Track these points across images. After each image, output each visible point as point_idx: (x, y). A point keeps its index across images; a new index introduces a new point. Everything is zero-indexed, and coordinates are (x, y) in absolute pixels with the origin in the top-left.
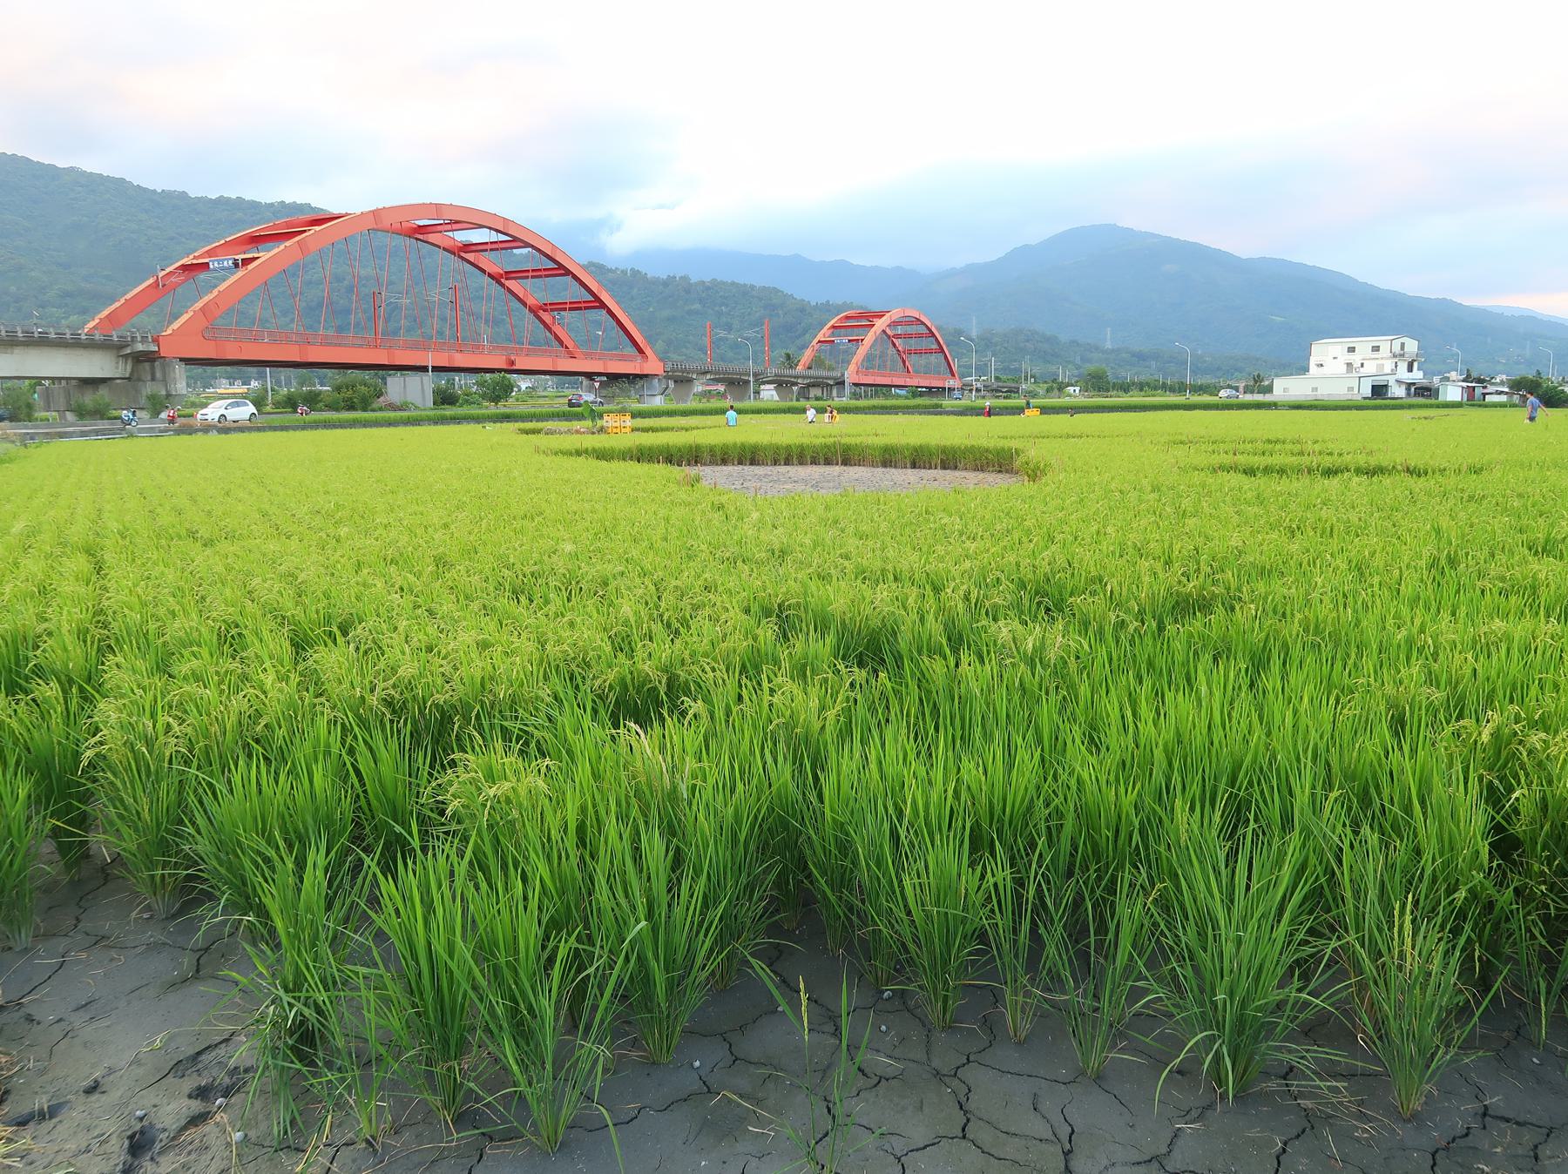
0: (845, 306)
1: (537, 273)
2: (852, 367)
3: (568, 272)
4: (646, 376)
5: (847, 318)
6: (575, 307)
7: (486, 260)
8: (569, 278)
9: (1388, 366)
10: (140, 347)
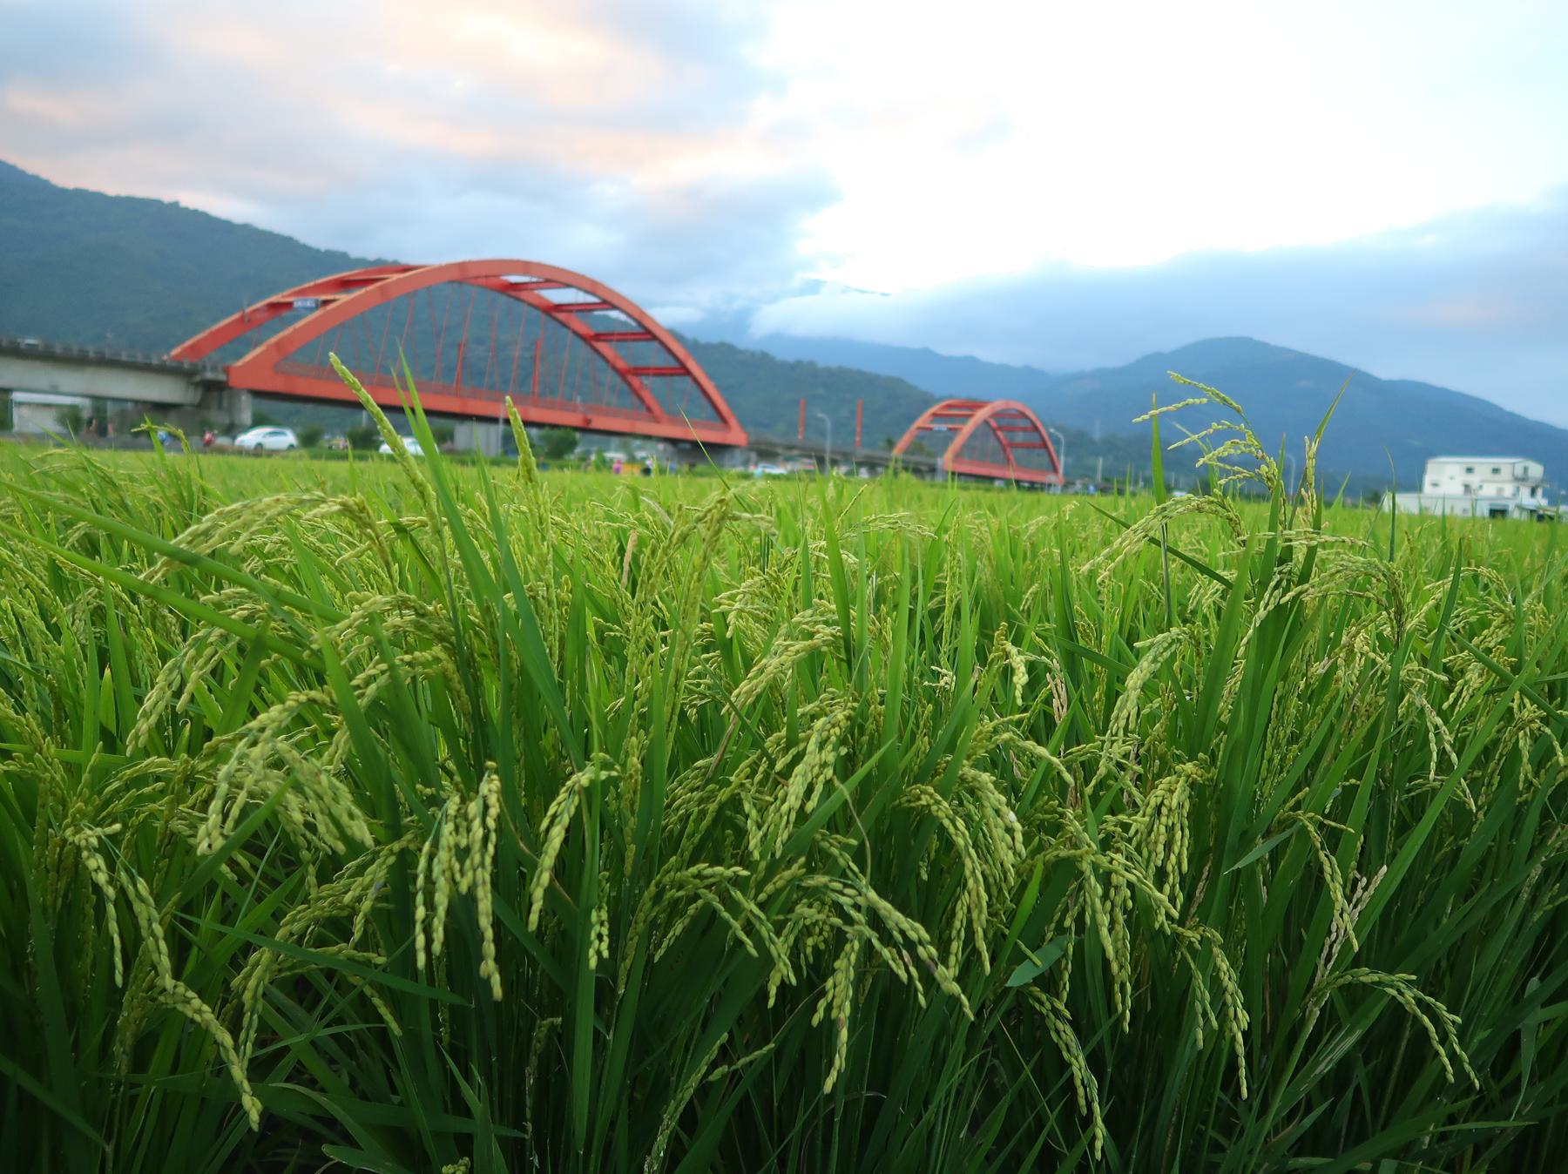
0: (951, 397)
1: (624, 337)
2: (949, 455)
5: (949, 407)
6: (660, 372)
7: (577, 322)
8: (655, 344)
9: (1509, 490)
10: (209, 375)
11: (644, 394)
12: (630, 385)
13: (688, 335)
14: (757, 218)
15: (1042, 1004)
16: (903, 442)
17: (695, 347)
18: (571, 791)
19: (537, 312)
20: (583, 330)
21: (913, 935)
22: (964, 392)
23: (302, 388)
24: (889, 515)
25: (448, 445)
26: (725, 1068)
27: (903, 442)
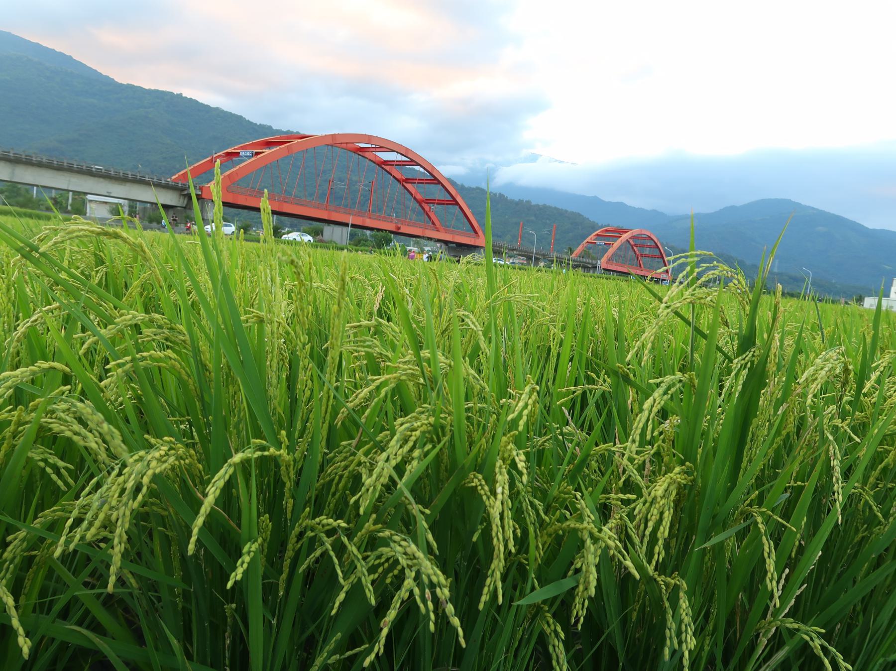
0: (608, 225)
1: (422, 181)
2: (604, 259)
3: (439, 183)
4: (478, 247)
5: (607, 231)
6: (441, 203)
7: (395, 171)
11: (431, 214)
12: (423, 209)
13: (459, 182)
14: (502, 117)
15: (549, 625)
16: (578, 250)
17: (462, 189)
18: (230, 466)
19: (373, 165)
20: (398, 176)
21: (434, 579)
22: (615, 223)
24: (549, 295)
25: (319, 237)
26: (338, 656)
27: (578, 250)
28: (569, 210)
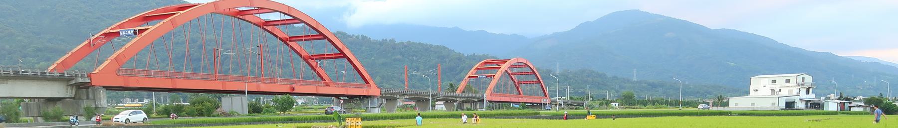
0: (485, 57)
2: (488, 91)
3: (325, 37)
4: (370, 96)
5: (485, 63)
6: (329, 57)
7: (278, 30)
9: (795, 91)
10: (80, 80)
11: (319, 70)
23: (179, 86)
28: (434, 43)
